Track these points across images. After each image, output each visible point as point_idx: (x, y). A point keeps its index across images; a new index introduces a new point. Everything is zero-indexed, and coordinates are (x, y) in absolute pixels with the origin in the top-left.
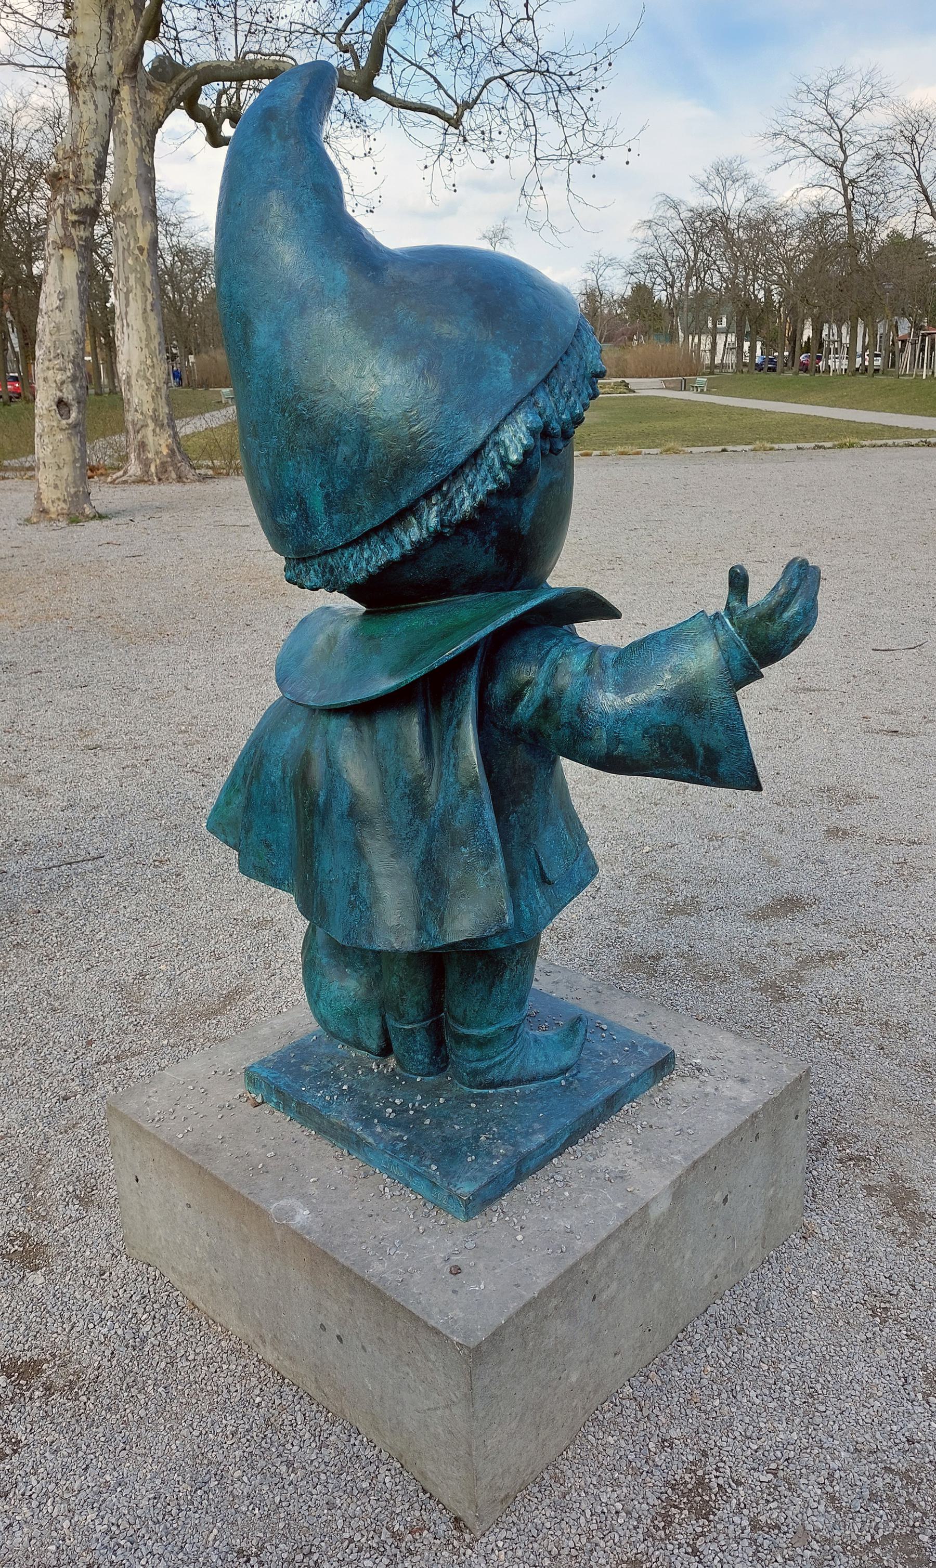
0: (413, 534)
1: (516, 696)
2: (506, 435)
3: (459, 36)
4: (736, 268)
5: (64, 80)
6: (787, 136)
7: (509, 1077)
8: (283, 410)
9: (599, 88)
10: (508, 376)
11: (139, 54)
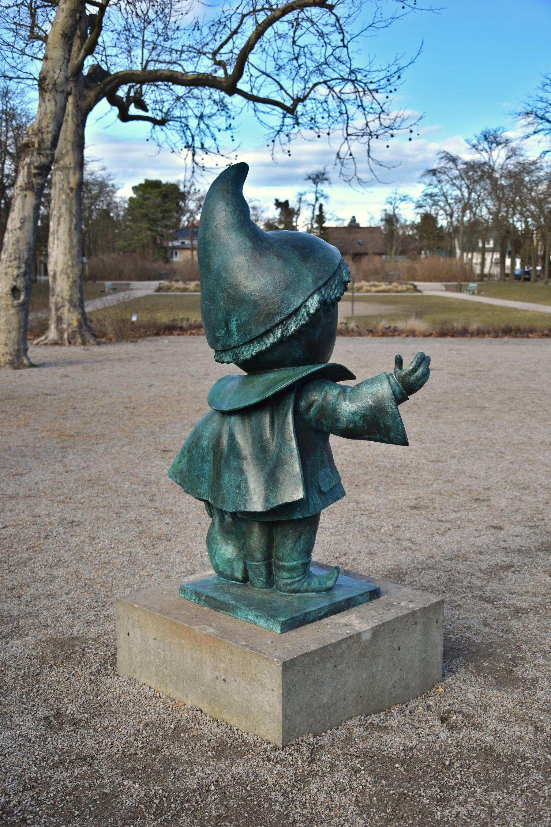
0: (271, 340)
1: (311, 405)
2: (308, 303)
3: (296, 59)
4: (500, 206)
5: (37, 87)
6: (537, 115)
7: (302, 589)
8: (223, 292)
9: (393, 90)
10: (311, 281)
11: (81, 66)
